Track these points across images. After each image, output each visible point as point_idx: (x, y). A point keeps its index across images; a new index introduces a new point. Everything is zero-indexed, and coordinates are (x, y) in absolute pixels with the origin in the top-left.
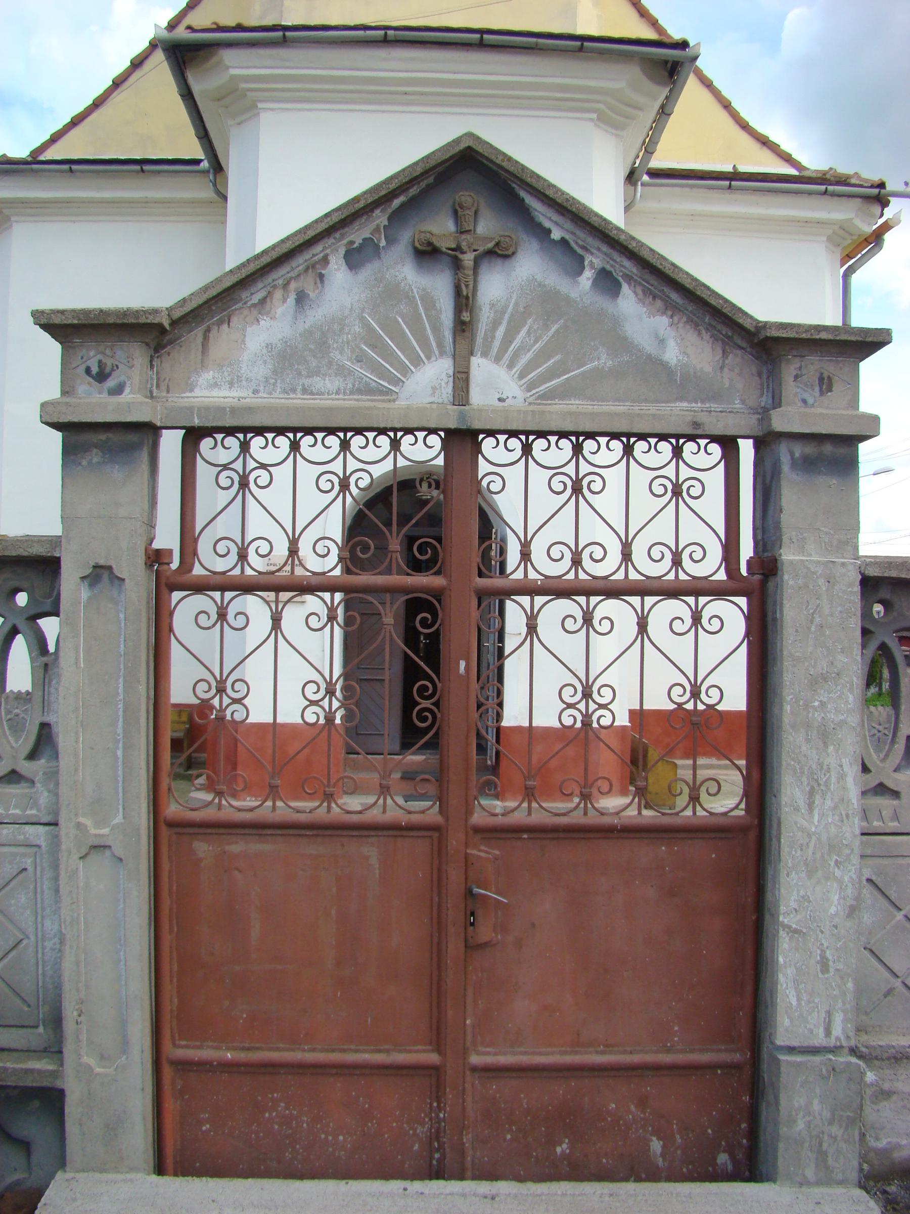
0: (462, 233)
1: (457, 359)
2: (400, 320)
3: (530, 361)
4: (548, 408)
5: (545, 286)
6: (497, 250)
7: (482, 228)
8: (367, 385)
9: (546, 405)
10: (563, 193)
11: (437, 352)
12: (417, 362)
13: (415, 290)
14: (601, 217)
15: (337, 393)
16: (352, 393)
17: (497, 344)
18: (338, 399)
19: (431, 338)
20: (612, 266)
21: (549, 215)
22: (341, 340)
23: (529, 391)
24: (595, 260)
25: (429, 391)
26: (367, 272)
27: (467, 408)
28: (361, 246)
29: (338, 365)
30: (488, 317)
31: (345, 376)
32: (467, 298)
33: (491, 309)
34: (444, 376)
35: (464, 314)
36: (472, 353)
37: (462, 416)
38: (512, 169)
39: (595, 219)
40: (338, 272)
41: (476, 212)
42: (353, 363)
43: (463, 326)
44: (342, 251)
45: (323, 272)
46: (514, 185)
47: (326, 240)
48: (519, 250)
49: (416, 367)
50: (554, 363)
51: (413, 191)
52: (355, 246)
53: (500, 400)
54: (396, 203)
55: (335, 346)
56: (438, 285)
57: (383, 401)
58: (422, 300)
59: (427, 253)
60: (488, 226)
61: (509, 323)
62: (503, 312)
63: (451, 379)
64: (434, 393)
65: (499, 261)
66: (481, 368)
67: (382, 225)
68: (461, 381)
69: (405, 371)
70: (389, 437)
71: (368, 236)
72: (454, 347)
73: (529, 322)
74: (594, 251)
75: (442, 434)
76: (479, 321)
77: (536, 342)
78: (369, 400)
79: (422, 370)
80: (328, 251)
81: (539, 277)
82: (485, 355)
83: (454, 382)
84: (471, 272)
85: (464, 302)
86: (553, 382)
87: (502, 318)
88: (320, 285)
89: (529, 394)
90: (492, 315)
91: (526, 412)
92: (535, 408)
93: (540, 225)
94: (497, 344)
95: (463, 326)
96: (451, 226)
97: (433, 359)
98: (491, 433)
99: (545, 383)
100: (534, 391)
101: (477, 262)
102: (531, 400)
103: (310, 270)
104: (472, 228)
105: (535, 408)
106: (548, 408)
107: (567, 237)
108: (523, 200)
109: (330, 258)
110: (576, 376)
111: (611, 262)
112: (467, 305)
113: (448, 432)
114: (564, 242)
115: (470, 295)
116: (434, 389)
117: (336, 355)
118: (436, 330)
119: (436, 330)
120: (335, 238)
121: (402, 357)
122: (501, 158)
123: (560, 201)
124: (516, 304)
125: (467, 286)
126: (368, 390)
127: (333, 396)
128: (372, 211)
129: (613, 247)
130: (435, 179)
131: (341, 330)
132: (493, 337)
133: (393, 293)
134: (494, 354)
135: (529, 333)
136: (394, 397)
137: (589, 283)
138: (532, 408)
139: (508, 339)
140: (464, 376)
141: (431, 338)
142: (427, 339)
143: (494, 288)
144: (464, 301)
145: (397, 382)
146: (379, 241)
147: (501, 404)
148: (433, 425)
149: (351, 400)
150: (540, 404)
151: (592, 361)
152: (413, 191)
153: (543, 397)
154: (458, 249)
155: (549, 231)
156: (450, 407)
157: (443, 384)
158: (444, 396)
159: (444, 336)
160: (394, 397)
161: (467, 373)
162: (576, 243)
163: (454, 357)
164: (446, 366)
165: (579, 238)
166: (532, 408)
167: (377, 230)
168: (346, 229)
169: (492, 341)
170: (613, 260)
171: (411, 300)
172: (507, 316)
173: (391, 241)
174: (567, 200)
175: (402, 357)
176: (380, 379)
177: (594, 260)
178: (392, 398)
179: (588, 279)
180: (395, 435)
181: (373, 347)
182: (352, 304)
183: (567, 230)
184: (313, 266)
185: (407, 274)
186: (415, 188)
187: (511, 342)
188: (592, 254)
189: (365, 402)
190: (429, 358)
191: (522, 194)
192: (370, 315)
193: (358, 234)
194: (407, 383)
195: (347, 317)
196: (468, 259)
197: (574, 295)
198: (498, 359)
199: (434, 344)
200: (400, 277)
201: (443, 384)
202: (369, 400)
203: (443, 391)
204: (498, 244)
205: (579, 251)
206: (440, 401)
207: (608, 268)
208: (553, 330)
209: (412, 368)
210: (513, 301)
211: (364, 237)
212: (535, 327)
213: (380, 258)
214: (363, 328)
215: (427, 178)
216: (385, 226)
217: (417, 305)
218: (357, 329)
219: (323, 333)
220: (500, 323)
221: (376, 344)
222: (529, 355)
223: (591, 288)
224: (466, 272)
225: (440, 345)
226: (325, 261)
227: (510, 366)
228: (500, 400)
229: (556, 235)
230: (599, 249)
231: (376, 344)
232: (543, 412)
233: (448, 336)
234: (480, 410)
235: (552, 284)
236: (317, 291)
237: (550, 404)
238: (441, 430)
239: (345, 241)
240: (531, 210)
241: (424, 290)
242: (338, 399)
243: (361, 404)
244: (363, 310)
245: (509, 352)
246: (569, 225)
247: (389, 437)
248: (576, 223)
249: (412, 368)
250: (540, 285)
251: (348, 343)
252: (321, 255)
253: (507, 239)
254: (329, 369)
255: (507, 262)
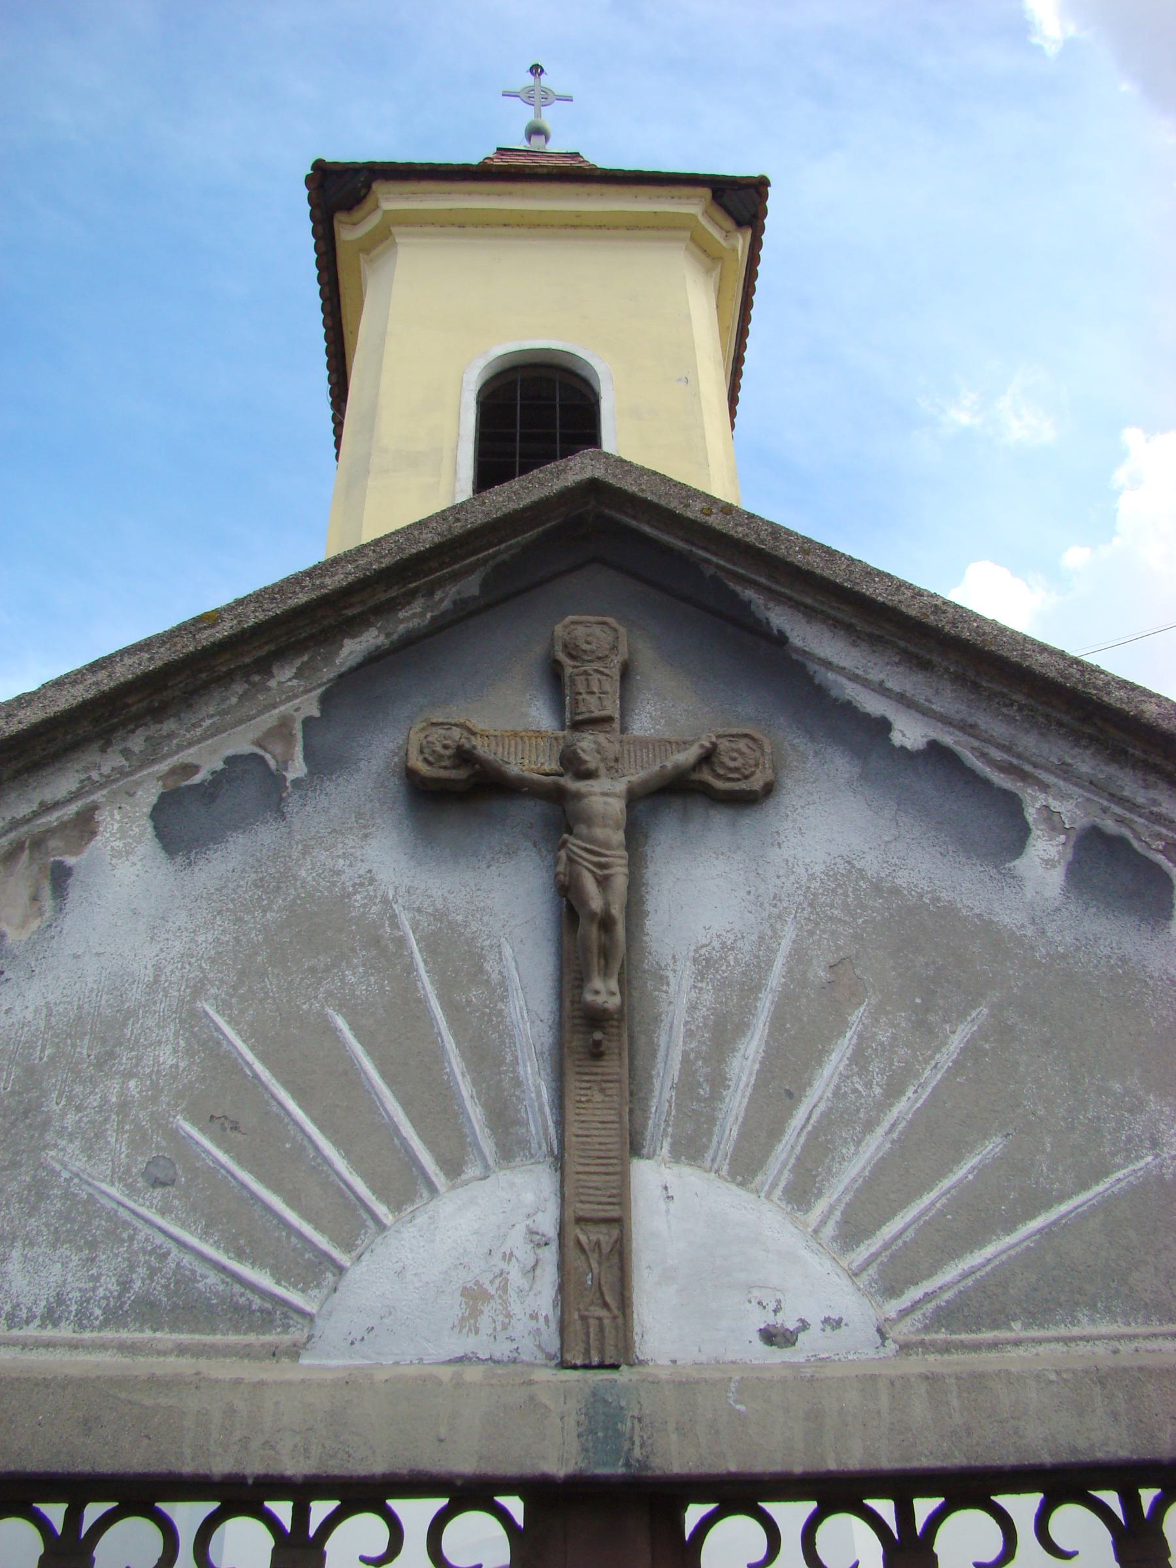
0: (578, 726)
1: (571, 1168)
2: (341, 1022)
3: (881, 1167)
4: (990, 1360)
5: (895, 891)
6: (706, 776)
7: (646, 722)
8: (183, 1281)
9: (976, 1347)
10: (918, 593)
11: (488, 1146)
12: (404, 1186)
13: (405, 919)
14: (1053, 652)
15: (51, 1317)
16: (114, 1317)
17: (735, 1103)
18: (49, 1345)
19: (466, 1088)
20: (1120, 821)
21: (875, 675)
22: (94, 1101)
23: (892, 1290)
24: (1058, 810)
25: (454, 1306)
26: (228, 861)
27: (624, 1375)
28: (218, 778)
29: (67, 1195)
30: (693, 1008)
31: (93, 1245)
32: (606, 923)
33: (701, 975)
34: (517, 1241)
35: (597, 983)
36: (635, 1147)
37: (603, 1419)
38: (739, 532)
39: (1043, 658)
40: (123, 864)
41: (626, 672)
42: (132, 1190)
43: (595, 1033)
44: (149, 795)
45: (70, 861)
46: (749, 594)
47: (91, 755)
48: (789, 783)
49: (397, 1207)
50: (981, 1171)
51: (413, 616)
52: (197, 779)
53: (770, 1336)
54: (352, 650)
55: (71, 1119)
56: (500, 902)
57: (246, 1353)
58: (431, 947)
59: (456, 795)
60: (669, 714)
61: (777, 1022)
62: (751, 988)
63: (550, 1255)
64: (475, 1313)
65: (719, 818)
66: (674, 1204)
67: (300, 717)
68: (595, 1258)
69: (352, 1223)
70: (272, 1522)
71: (247, 748)
72: (561, 1124)
73: (857, 1017)
74: (1050, 779)
75: (515, 1505)
76: (657, 1019)
77: (894, 1091)
78: (182, 1350)
79: (422, 1219)
80: (98, 796)
81: (871, 864)
82: (690, 1149)
83: (562, 1266)
84: (619, 837)
85: (592, 939)
86: (989, 1251)
87: (747, 1009)
88: (48, 903)
89: (893, 1307)
90: (708, 998)
91: (900, 1385)
92: (933, 1362)
93: (848, 709)
94: (735, 1103)
95: (595, 1033)
96: (539, 715)
97: (471, 1171)
98: (741, 1494)
99: (956, 1254)
100: (914, 1293)
101: (635, 835)
102: (905, 1330)
103: (25, 856)
104: (612, 708)
105: (933, 1362)
106: (990, 1360)
107: (948, 738)
108: (781, 640)
109: (102, 816)
110: (1080, 1218)
111: (1118, 810)
112: (606, 953)
113: (536, 1490)
114: (936, 752)
115: (617, 911)
116: (474, 1296)
117: (67, 1157)
118: (487, 1057)
119: (487, 1057)
120: (126, 753)
121: (341, 1164)
122: (698, 505)
123: (913, 612)
124: (799, 955)
125: (603, 882)
126: (185, 1306)
127: (32, 1331)
128: (264, 666)
129: (1118, 755)
130: (485, 585)
131: (104, 1061)
132: (719, 1081)
133: (321, 930)
134: (728, 1147)
135: (859, 1058)
136: (298, 1334)
137: (1056, 878)
138: (915, 1364)
139: (780, 1085)
140: (604, 1236)
141: (466, 1088)
142: (447, 1094)
143: (704, 904)
144: (594, 932)
145: (316, 1269)
146: (284, 764)
147: (776, 1356)
148: (464, 1463)
149: (103, 1346)
150: (946, 1348)
151: (1130, 1152)
152: (413, 616)
153: (955, 1313)
154: (572, 763)
155: (883, 726)
156: (547, 1375)
157: (516, 1278)
158: (521, 1326)
159: (518, 1083)
160: (298, 1334)
161: (619, 1223)
162: (983, 756)
163: (560, 1162)
164: (529, 1197)
165: (989, 741)
166: (915, 1364)
167: (282, 729)
168: (170, 725)
169: (715, 1097)
170: (1121, 801)
171: (386, 952)
172: (765, 1005)
173: (324, 764)
174: (936, 609)
175: (341, 1164)
176: (240, 1255)
177: (1055, 805)
178: (287, 1339)
179: (1049, 863)
180: (301, 1515)
181: (223, 1126)
182: (158, 968)
183: (944, 720)
184: (38, 843)
185: (375, 862)
186: (417, 606)
187: (793, 1097)
188: (1044, 787)
189: (163, 1353)
190: (453, 1168)
191: (780, 618)
192: (224, 1007)
193: (209, 743)
194: (357, 1274)
195: (131, 1014)
196: (605, 798)
197: (1009, 915)
198: (744, 1168)
199: (475, 1113)
200: (349, 876)
201: (516, 1278)
202: (182, 1350)
203: (516, 1308)
204: (708, 758)
205: (999, 779)
206: (502, 1349)
207: (1110, 826)
208: (956, 1042)
209: (381, 1209)
210: (785, 946)
211: (230, 752)
212: (884, 1036)
213: (283, 816)
214: (190, 1052)
215: (456, 577)
216: (308, 722)
217: (410, 968)
218: (166, 1057)
219: (30, 1071)
220: (742, 1028)
221: (231, 1108)
222: (874, 1144)
223: (1065, 892)
224: (599, 832)
225: (503, 1118)
226: (84, 826)
227: (800, 1193)
228: (770, 1336)
229: (909, 733)
230: (1065, 771)
231: (231, 1108)
232: (976, 1381)
233: (534, 1079)
234: (686, 1386)
235: (924, 885)
236: (35, 924)
237: (994, 1345)
238: (510, 1486)
239: (164, 767)
240: (812, 667)
241: (439, 916)
242: (49, 1345)
243: (144, 1365)
244: (198, 990)
245: (789, 1136)
246: (948, 701)
247: (272, 1522)
248: (976, 687)
249: (381, 1209)
250: (877, 888)
251: (124, 1106)
252: (73, 809)
253: (742, 745)
254: (33, 1210)
255: (749, 821)
